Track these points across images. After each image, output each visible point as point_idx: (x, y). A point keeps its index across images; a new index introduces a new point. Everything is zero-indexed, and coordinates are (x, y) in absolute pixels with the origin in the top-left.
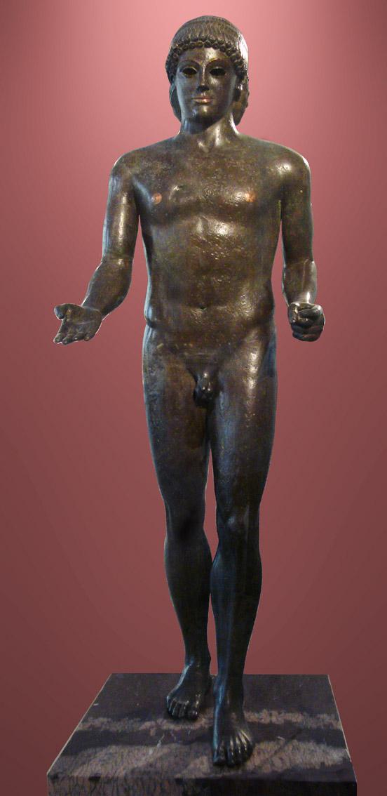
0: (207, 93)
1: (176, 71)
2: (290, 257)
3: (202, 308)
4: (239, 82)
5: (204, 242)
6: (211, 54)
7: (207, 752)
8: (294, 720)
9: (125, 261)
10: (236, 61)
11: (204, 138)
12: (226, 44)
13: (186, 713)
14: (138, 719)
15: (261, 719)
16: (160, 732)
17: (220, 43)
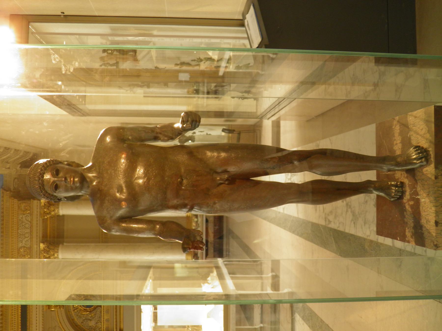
1: (55, 196)
2: (156, 139)
3: (183, 180)
5: (147, 179)
7: (420, 170)
8: (398, 131)
9: (158, 224)
11: (92, 181)
12: (42, 167)
13: (400, 187)
14: (405, 213)
15: (399, 148)
16: (412, 199)
17: (42, 170)
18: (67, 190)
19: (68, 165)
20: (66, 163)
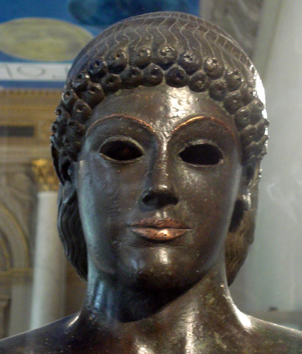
0: (173, 213)
4: (244, 185)
6: (181, 104)
10: (249, 127)
12: (229, 79)
17: (212, 74)
18: (107, 207)
19: (240, 205)
20: (247, 198)
